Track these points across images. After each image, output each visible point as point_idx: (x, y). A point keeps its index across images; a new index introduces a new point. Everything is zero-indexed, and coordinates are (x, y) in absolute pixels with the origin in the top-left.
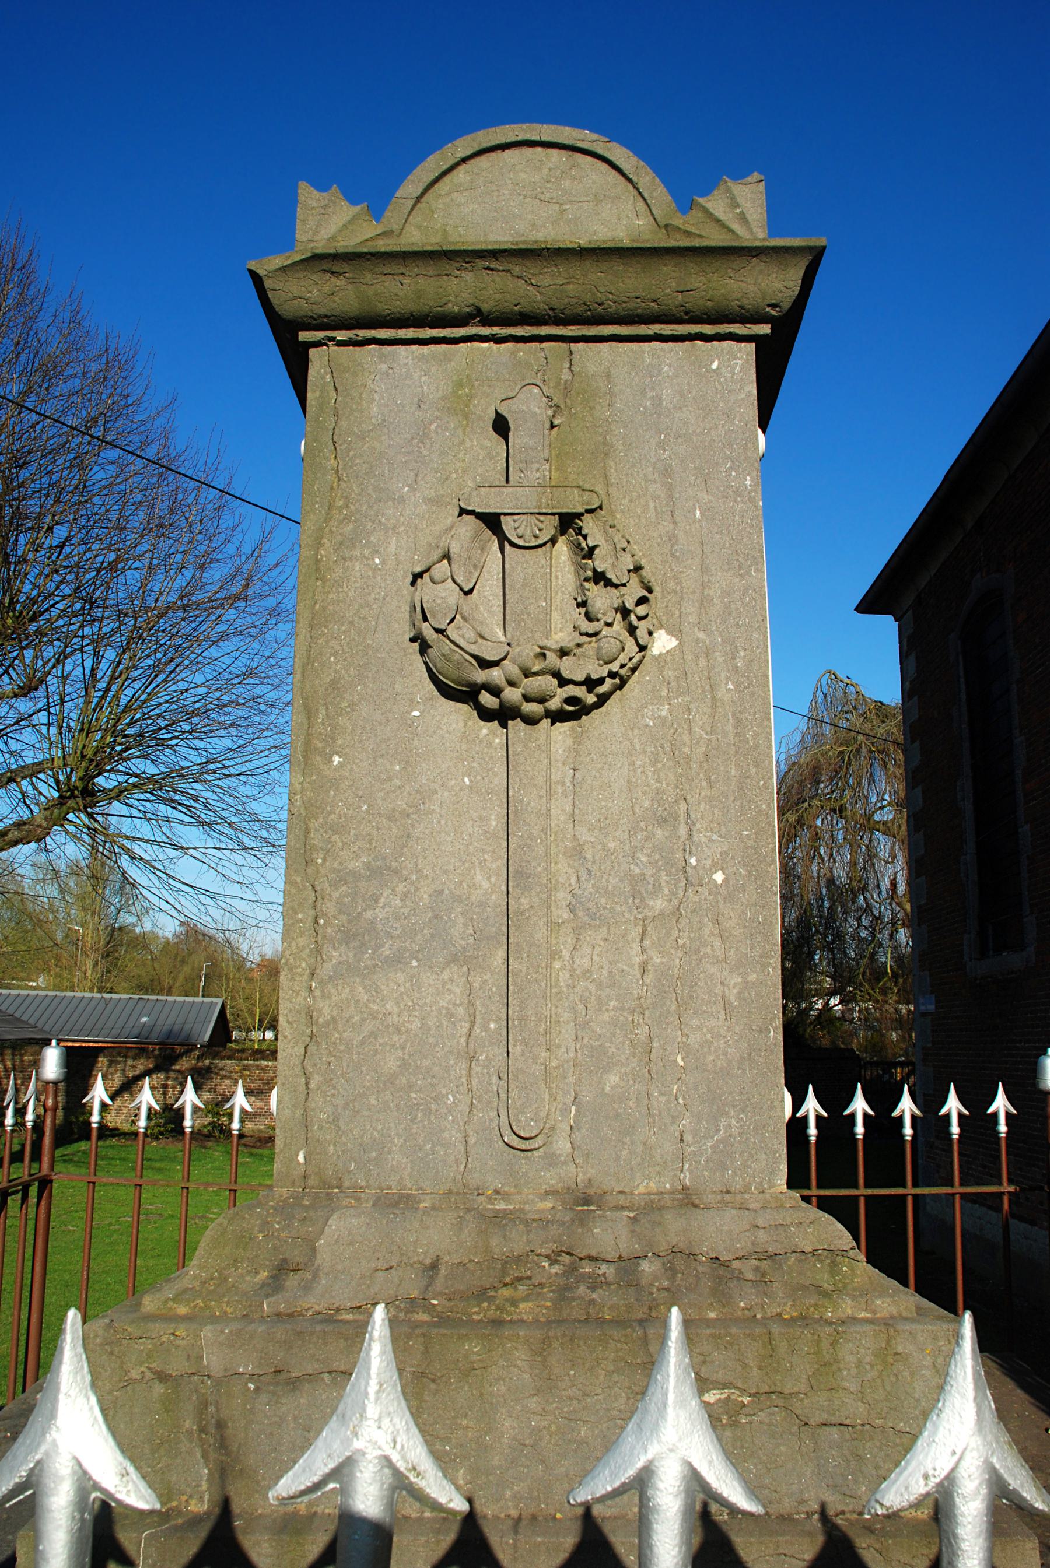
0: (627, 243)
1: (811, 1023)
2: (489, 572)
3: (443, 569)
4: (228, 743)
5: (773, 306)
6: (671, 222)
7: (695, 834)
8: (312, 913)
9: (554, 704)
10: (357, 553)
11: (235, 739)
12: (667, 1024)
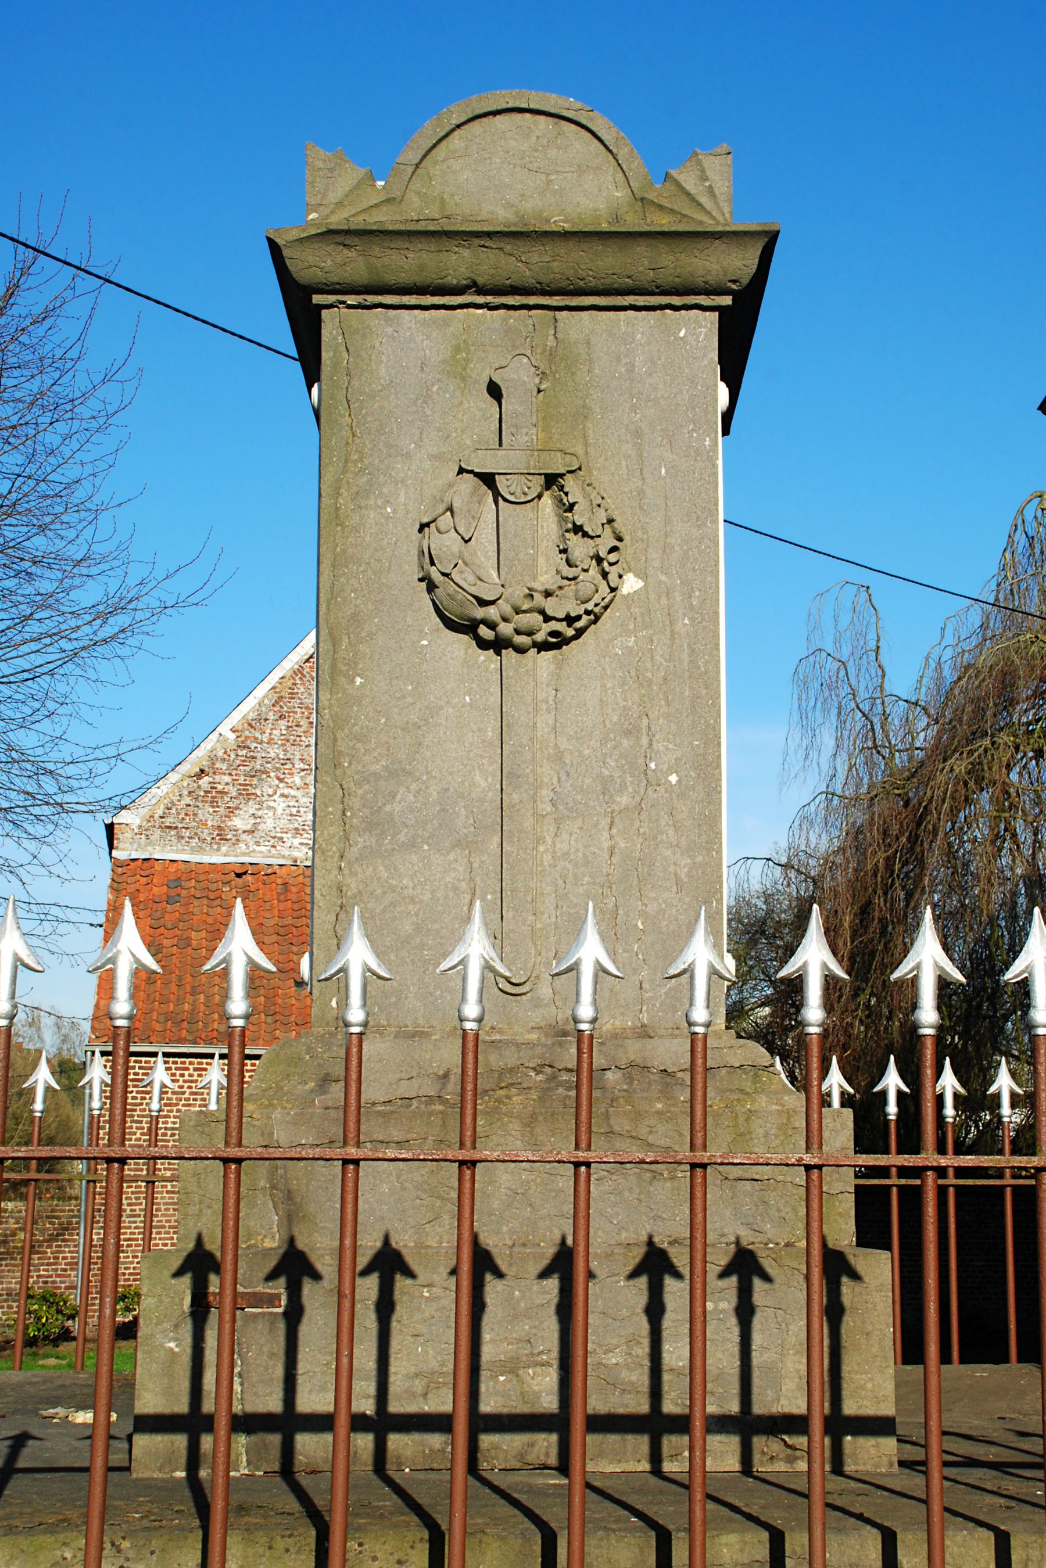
2: (485, 522)
5: (734, 281)
6: (647, 196)
7: (654, 743)
9: (540, 637)
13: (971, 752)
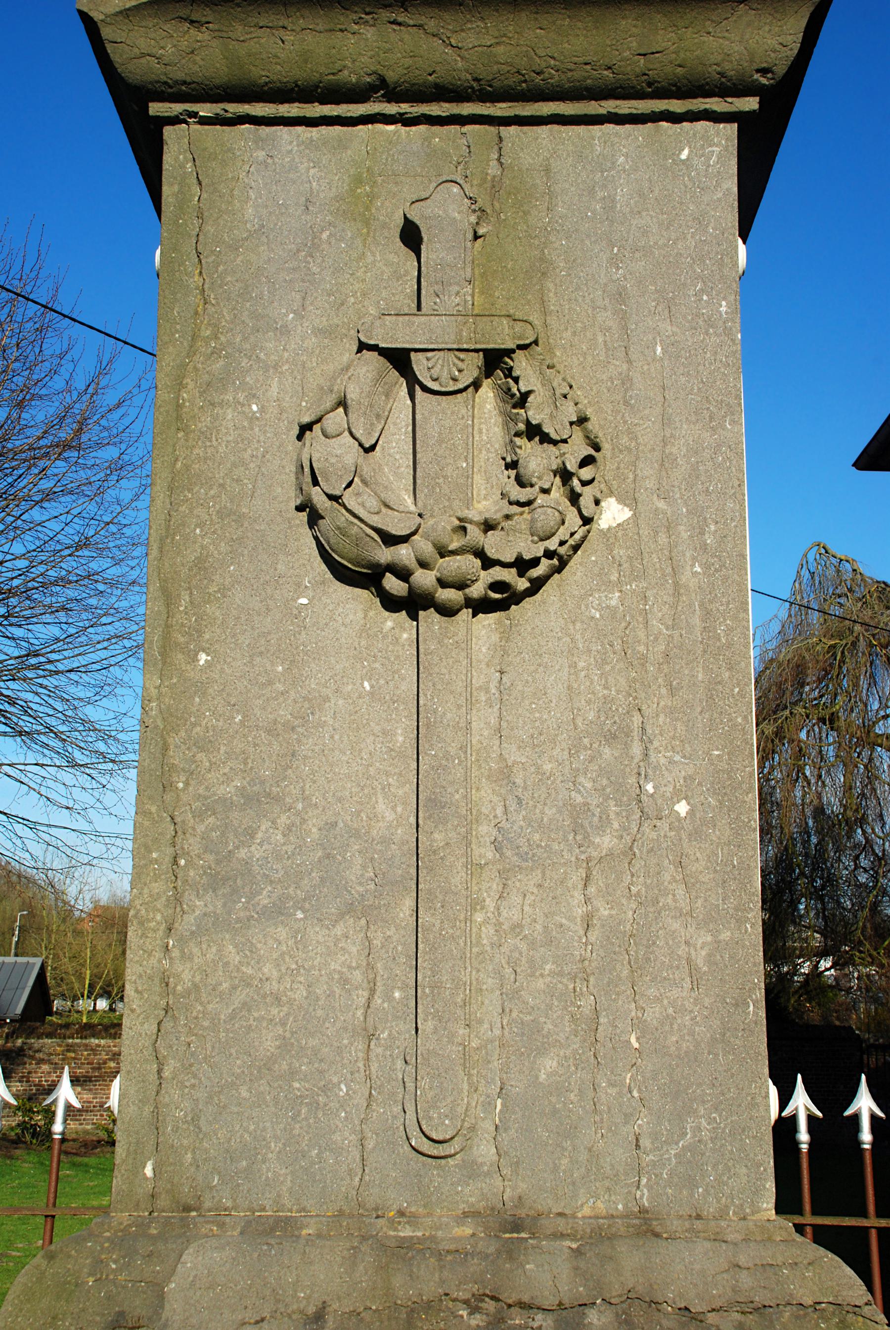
1: (796, 992)
2: (395, 424)
3: (338, 420)
4: (55, 631)
5: (764, 71)
8: (170, 851)
9: (477, 590)
10: (229, 397)
11: (64, 626)
12: (618, 994)
13: (775, 720)
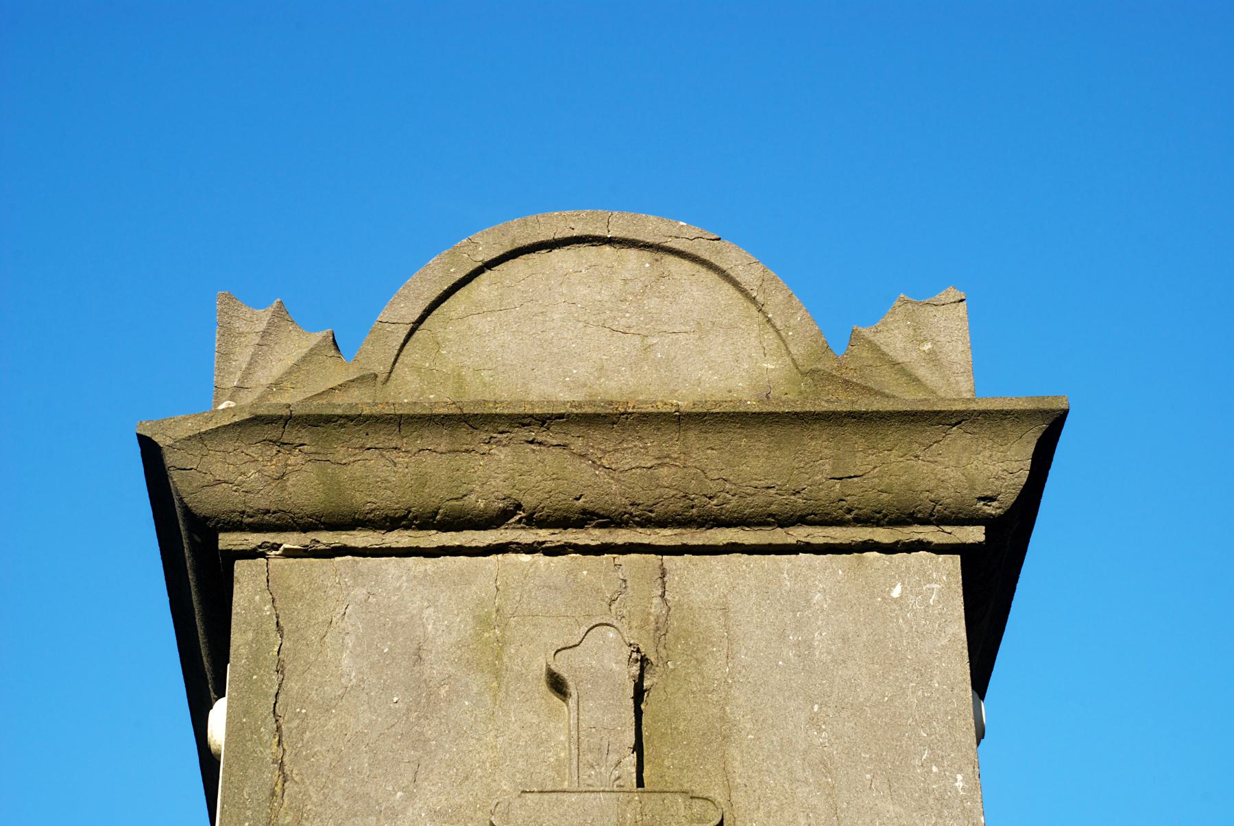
0: (753, 406)
5: (988, 499)
